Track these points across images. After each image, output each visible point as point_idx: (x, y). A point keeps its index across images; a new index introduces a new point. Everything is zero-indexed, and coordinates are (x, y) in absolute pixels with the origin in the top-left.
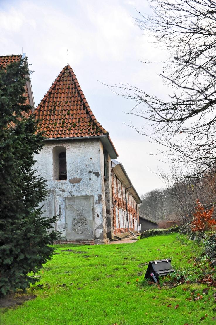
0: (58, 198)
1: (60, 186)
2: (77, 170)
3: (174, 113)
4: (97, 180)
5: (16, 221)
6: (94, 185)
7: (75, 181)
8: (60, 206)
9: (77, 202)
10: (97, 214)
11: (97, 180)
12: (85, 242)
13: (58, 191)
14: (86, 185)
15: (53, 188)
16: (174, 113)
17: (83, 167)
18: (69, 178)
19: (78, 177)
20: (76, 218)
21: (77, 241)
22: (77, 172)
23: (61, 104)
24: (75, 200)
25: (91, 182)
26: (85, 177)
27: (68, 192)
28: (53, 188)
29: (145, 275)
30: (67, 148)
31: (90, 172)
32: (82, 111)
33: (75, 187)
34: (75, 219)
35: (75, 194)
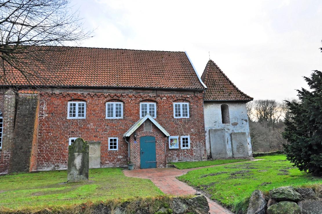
0: (226, 133)
1: (227, 127)
2: (235, 118)
3: (15, 11)
5: (291, 143)
7: (235, 124)
8: (227, 138)
13: (226, 130)
14: (241, 127)
15: (223, 127)
16: (15, 11)
18: (231, 123)
19: (236, 122)
20: (238, 145)
22: (235, 119)
23: (217, 81)
24: (237, 135)
25: (243, 125)
26: (239, 122)
28: (223, 127)
30: (229, 105)
31: (242, 120)
32: (230, 86)
33: (235, 128)
35: (235, 131)
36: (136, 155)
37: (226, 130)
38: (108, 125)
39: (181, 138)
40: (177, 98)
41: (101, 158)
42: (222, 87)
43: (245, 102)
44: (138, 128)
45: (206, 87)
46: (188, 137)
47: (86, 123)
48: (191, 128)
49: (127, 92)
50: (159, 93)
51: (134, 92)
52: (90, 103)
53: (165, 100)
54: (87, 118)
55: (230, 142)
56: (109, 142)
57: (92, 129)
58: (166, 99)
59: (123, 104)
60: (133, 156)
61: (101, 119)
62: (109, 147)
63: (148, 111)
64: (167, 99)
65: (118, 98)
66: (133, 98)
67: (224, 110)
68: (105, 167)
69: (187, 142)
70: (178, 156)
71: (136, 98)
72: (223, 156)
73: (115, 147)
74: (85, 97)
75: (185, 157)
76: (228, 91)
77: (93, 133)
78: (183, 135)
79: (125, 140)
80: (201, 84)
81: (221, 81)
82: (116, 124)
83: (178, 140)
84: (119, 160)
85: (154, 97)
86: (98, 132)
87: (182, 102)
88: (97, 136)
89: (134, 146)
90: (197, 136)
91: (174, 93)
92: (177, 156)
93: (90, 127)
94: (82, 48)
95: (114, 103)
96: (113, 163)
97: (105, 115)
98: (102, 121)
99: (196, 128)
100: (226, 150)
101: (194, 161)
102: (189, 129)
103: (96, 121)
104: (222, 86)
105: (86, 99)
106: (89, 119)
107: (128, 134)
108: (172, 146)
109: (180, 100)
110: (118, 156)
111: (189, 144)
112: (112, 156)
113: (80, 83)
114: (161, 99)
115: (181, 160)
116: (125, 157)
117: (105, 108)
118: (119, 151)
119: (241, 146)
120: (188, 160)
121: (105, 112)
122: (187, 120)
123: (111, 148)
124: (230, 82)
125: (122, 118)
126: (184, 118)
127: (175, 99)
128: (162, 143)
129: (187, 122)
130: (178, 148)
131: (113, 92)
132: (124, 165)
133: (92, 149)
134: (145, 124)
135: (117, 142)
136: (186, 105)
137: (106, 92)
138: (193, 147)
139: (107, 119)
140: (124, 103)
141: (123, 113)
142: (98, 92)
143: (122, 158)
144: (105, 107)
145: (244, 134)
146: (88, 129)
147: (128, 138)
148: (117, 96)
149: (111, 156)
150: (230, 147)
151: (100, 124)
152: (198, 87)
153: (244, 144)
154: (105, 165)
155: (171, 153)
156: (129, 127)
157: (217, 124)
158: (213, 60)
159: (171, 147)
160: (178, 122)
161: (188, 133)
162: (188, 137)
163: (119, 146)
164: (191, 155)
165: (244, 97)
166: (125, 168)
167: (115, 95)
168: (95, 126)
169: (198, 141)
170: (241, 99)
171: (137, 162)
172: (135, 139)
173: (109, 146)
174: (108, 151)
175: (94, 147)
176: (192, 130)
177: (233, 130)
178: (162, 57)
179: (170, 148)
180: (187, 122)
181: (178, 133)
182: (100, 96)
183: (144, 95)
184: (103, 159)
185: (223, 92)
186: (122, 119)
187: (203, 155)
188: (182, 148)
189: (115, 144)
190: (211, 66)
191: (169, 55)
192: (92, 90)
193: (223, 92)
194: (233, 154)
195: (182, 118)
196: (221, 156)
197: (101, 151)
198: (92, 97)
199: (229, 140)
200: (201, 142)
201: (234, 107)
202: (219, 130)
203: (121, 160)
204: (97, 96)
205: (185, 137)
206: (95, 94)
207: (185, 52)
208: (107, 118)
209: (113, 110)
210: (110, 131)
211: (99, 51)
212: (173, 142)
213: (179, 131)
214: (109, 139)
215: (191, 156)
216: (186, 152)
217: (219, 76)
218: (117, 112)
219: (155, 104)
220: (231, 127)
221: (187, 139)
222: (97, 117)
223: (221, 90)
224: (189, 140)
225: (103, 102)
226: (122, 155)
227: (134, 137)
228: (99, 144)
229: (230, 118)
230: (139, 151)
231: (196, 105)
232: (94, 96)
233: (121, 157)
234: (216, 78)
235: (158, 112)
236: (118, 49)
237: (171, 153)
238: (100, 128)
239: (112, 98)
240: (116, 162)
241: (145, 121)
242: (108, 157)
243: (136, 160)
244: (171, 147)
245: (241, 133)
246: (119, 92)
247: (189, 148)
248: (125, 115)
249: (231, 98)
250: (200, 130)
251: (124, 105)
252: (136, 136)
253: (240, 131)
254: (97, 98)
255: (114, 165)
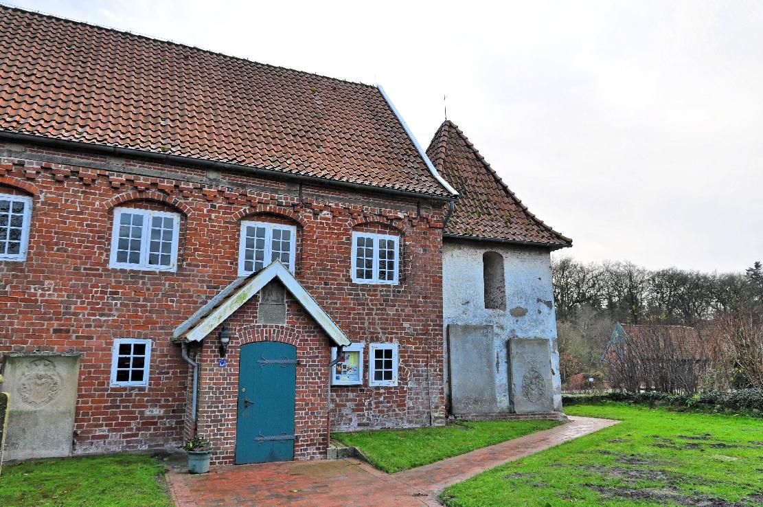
2: (520, 294)
4: (549, 314)
6: (545, 322)
9: (528, 348)
10: (552, 371)
11: (549, 314)
12: (546, 417)
13: (496, 330)
14: (536, 321)
15: (486, 321)
17: (529, 291)
18: (509, 308)
19: (522, 306)
21: (532, 415)
22: (521, 298)
24: (526, 346)
25: (541, 317)
26: (531, 307)
27: (508, 330)
28: (486, 321)
29: (7, 195)
30: (504, 256)
31: (539, 300)
32: (506, 200)
33: (518, 323)
34: (525, 377)
35: (520, 335)
36: (221, 411)
37: (496, 330)
38: (117, 293)
39: (370, 348)
40: (365, 217)
41: (77, 414)
42: (484, 202)
43: (546, 249)
44: (235, 309)
45: (455, 192)
46: (394, 347)
47: (26, 277)
48: (403, 320)
49: (196, 177)
50: (308, 194)
51: (224, 182)
52: (50, 205)
53: (329, 219)
54: (29, 259)
55: (503, 367)
56: (116, 355)
57: (49, 303)
58: (330, 216)
59: (182, 219)
60: (208, 417)
61: (88, 266)
62: (114, 375)
63: (269, 253)
64: (334, 216)
65: (164, 197)
66: (220, 203)
67: (490, 264)
68: (92, 450)
69: (389, 364)
70: (358, 408)
71: (229, 203)
72: (486, 408)
73: (138, 376)
74: (29, 179)
75: (379, 411)
76: (503, 213)
77: (51, 319)
78: (377, 340)
79: (184, 352)
80: (439, 183)
81: (481, 184)
82: (148, 289)
83: (362, 355)
84: (148, 423)
85: (294, 205)
86: (75, 314)
87: (379, 232)
88: (68, 331)
89: (216, 379)
90: (421, 344)
91: (356, 201)
92: (354, 410)
93: (42, 295)
94: (36, 17)
95: (148, 215)
96: (125, 436)
97: (108, 256)
98: (94, 275)
99: (419, 321)
100: (493, 389)
101: (407, 426)
102: (397, 321)
103: (68, 273)
104: (485, 198)
105: (32, 187)
106: (39, 265)
107: (196, 335)
108: (342, 376)
109: (373, 224)
110: (146, 407)
111: (395, 370)
112: (124, 407)
113: (14, 124)
114: (316, 215)
115: (367, 425)
116: (174, 411)
117: (110, 229)
118: (150, 389)
119: (535, 379)
120: (388, 425)
121: (109, 244)
122: (394, 291)
123: (122, 376)
124: (505, 188)
125: (174, 270)
126: (383, 286)
127: (361, 219)
128: (320, 370)
129: (392, 298)
130: (361, 382)
131: (145, 174)
132: (166, 441)
133: (39, 382)
134: (263, 299)
135: (147, 356)
136: (391, 244)
137: (119, 171)
138: (406, 379)
139: (114, 270)
140: (184, 216)
141: (179, 250)
142: (86, 167)
143: (160, 418)
144: (111, 224)
145: (542, 342)
146: (31, 301)
147: (195, 346)
148: (161, 191)
149: (118, 407)
150: (505, 381)
151: (84, 286)
152: (426, 188)
153: (542, 371)
154: (92, 444)
155: (338, 399)
156: (195, 303)
157: (471, 307)
158: (455, 123)
159: (337, 378)
160: (364, 295)
161: (392, 333)
162: (394, 347)
163: (151, 373)
164: (398, 406)
165: (546, 234)
166: (175, 458)
167: (154, 184)
168: (61, 290)
169: (422, 362)
170: (535, 240)
171: (225, 439)
172: (222, 351)
173: (114, 369)
174: (107, 390)
175: (49, 374)
176: (406, 325)
177: (513, 331)
178: (314, 92)
179: (335, 382)
180: (392, 298)
181: (364, 333)
182: (94, 181)
183: (259, 195)
184: (83, 420)
185: (489, 214)
186: (173, 274)
187: (437, 407)
188: (373, 383)
189: (139, 363)
190: (449, 135)
191: (335, 89)
192: (60, 156)
193: (489, 214)
194: (511, 402)
195: (377, 286)
196: (478, 408)
197: (79, 390)
198: (61, 182)
199: (503, 360)
200: (431, 366)
201: (517, 261)
202: (476, 328)
203: (155, 423)
204: (81, 179)
205: (384, 347)
206: (75, 173)
207: (377, 89)
208: (114, 264)
209: (143, 235)
210: (124, 316)
211: (93, 95)
212: (344, 363)
213: (366, 325)
214: (117, 342)
215: (398, 412)
216: (385, 398)
217: (475, 170)
218: (154, 246)
219: (293, 230)
220: (508, 321)
221: (389, 353)
222: (74, 257)
223: (481, 208)
224: (395, 359)
225: (101, 205)
226: (161, 407)
227: (220, 342)
228: (74, 364)
229: (507, 292)
230: (234, 397)
231: (422, 246)
232: (67, 177)
233: (157, 412)
234: (466, 175)
235: (302, 259)
236: (169, 43)
237: (338, 399)
238: (83, 303)
239: (141, 192)
240: (138, 429)
241: (264, 288)
242: (106, 413)
243: (219, 426)
244: (337, 378)
245: (536, 339)
246: (168, 177)
247: (394, 382)
248: (183, 260)
249: (514, 234)
250: (430, 325)
251: (182, 225)
252: (225, 340)
253: (531, 335)
254: (81, 187)
255: (128, 442)
